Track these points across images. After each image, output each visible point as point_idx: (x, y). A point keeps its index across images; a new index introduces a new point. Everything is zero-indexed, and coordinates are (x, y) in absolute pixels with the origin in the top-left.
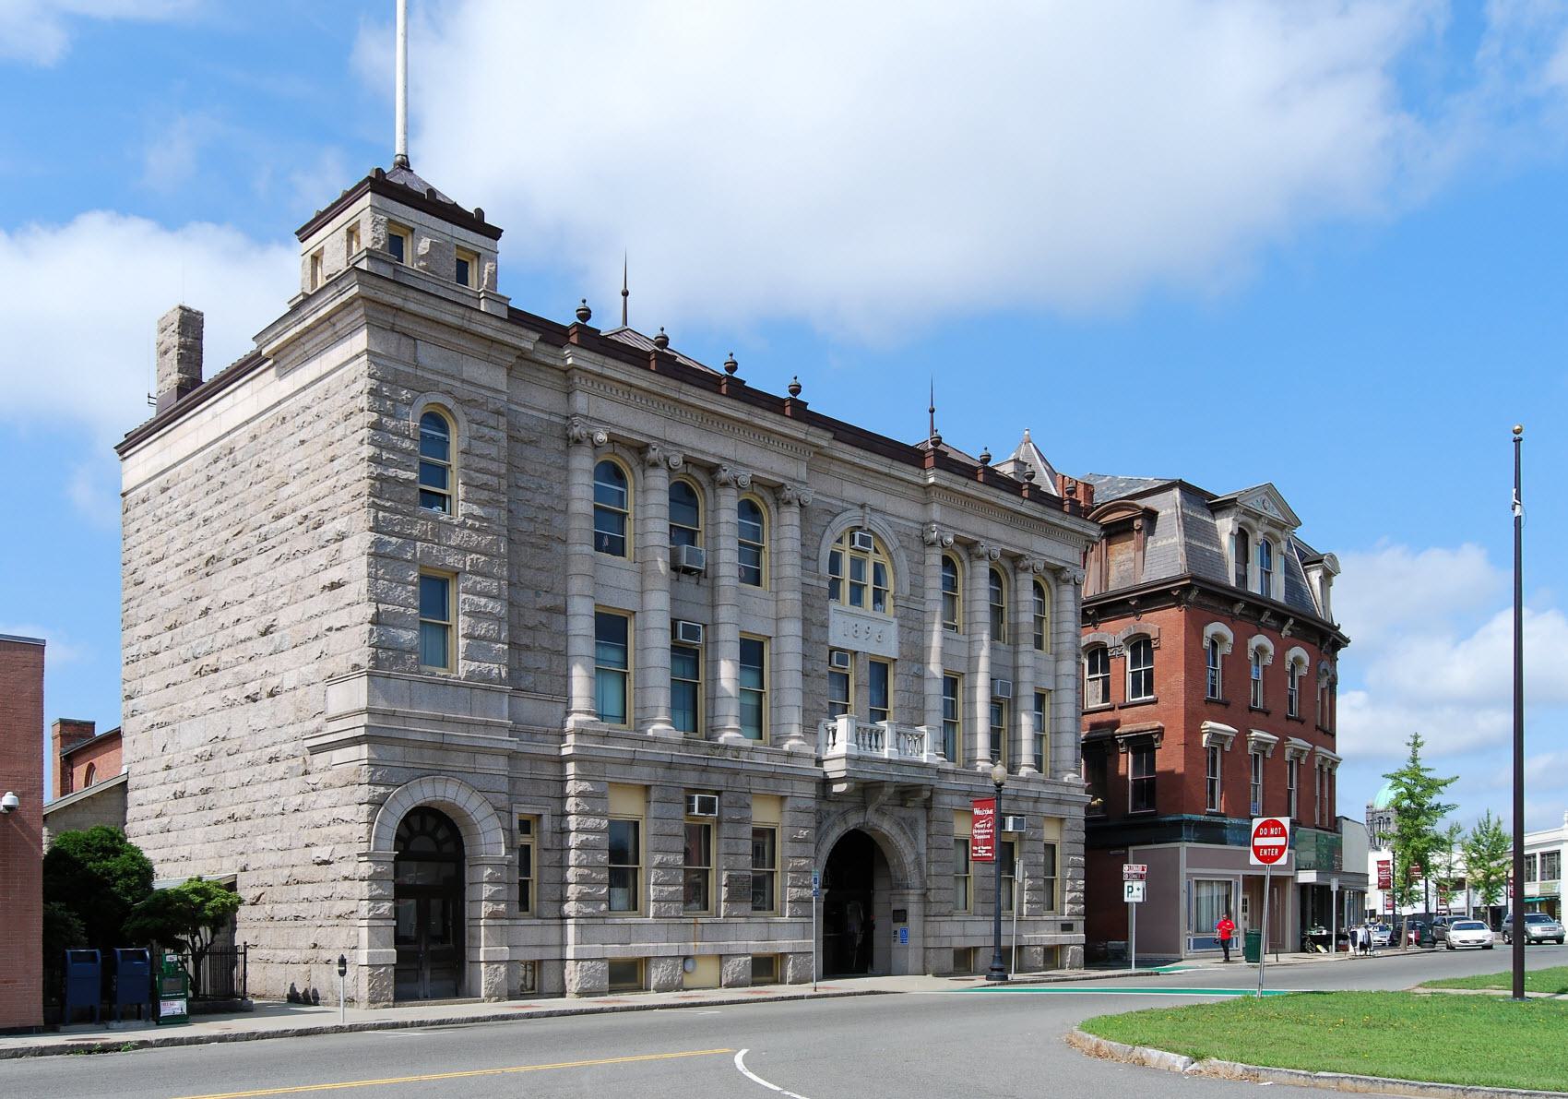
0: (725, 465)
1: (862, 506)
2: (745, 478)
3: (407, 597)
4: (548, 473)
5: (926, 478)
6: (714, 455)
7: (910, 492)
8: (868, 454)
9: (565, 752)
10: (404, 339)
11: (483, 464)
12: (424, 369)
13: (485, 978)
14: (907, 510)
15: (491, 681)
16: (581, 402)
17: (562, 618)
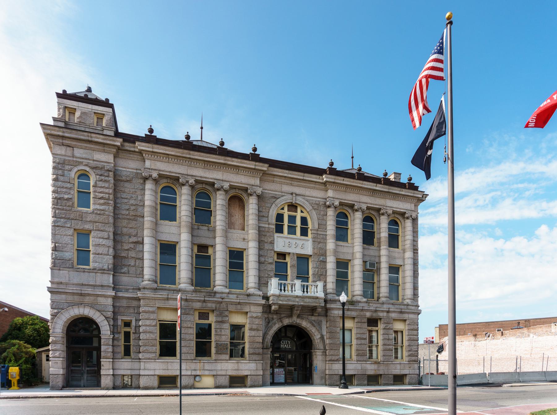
0: (356, 204)
1: (292, 194)
2: (364, 207)
3: (70, 241)
4: (136, 192)
5: (323, 179)
6: (211, 178)
7: (317, 186)
8: (291, 172)
9: (271, 302)
10: (68, 148)
11: (102, 190)
12: (76, 157)
13: (105, 380)
14: (317, 194)
15: (104, 270)
16: (148, 164)
17: (141, 245)
